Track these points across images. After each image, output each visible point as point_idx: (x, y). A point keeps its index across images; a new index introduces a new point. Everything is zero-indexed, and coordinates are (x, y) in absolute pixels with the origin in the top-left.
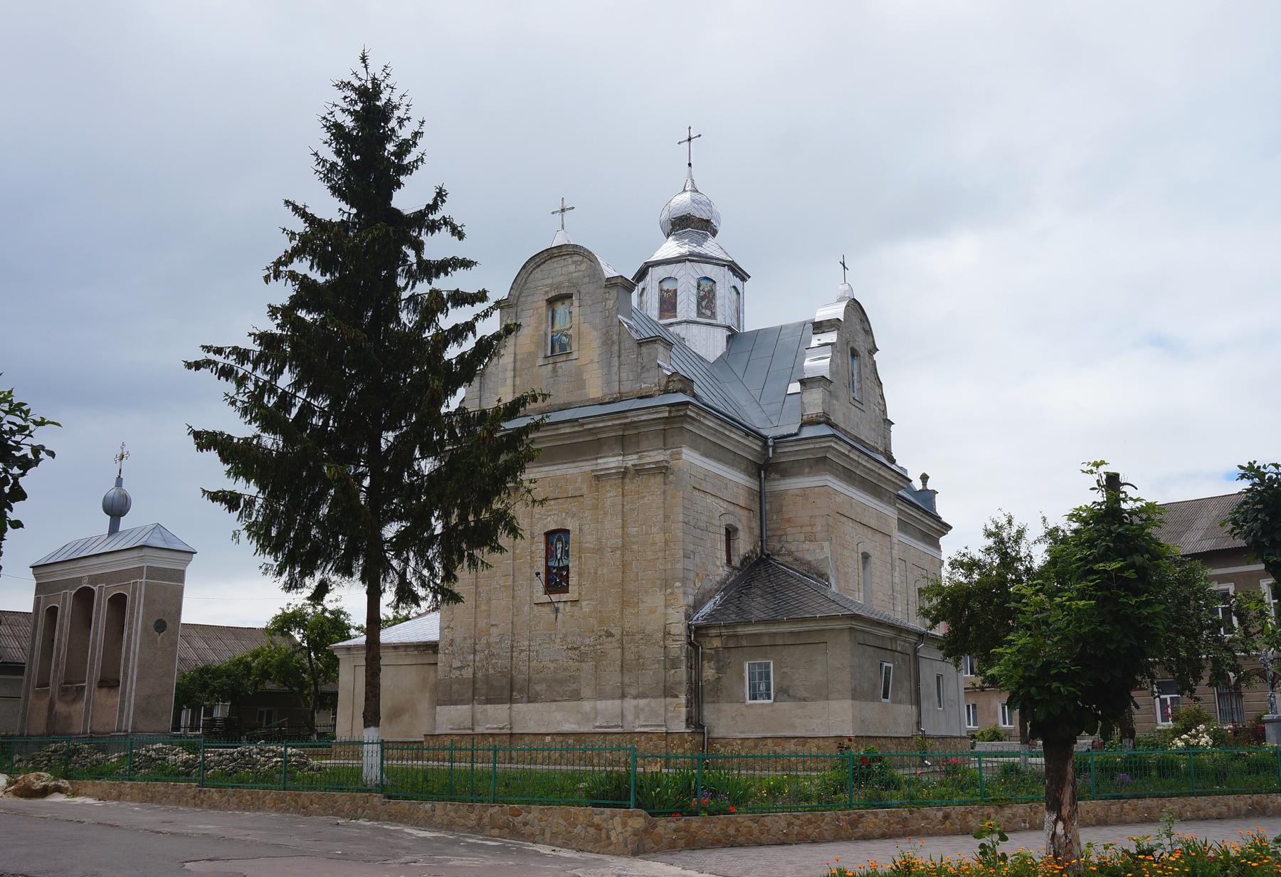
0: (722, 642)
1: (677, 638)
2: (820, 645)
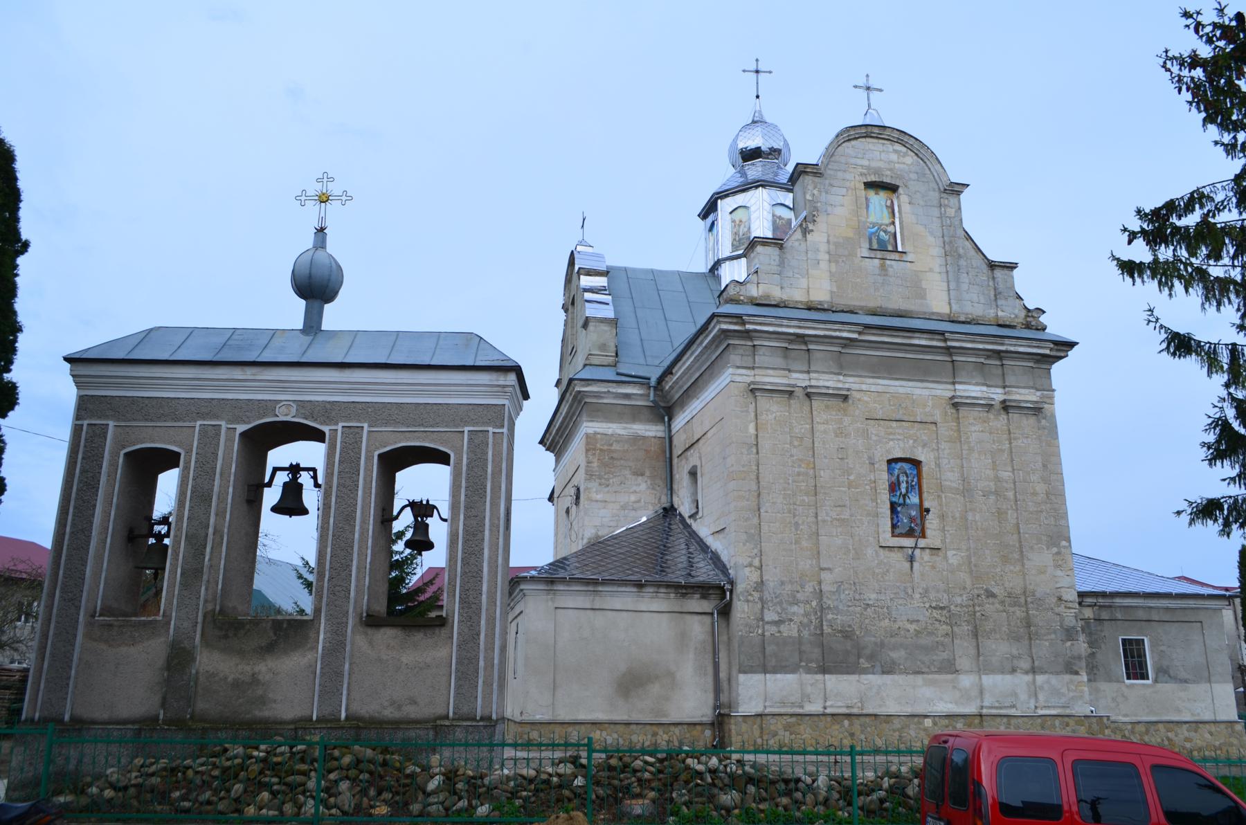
0: (1094, 612)
1: (1070, 605)
2: (1194, 624)
